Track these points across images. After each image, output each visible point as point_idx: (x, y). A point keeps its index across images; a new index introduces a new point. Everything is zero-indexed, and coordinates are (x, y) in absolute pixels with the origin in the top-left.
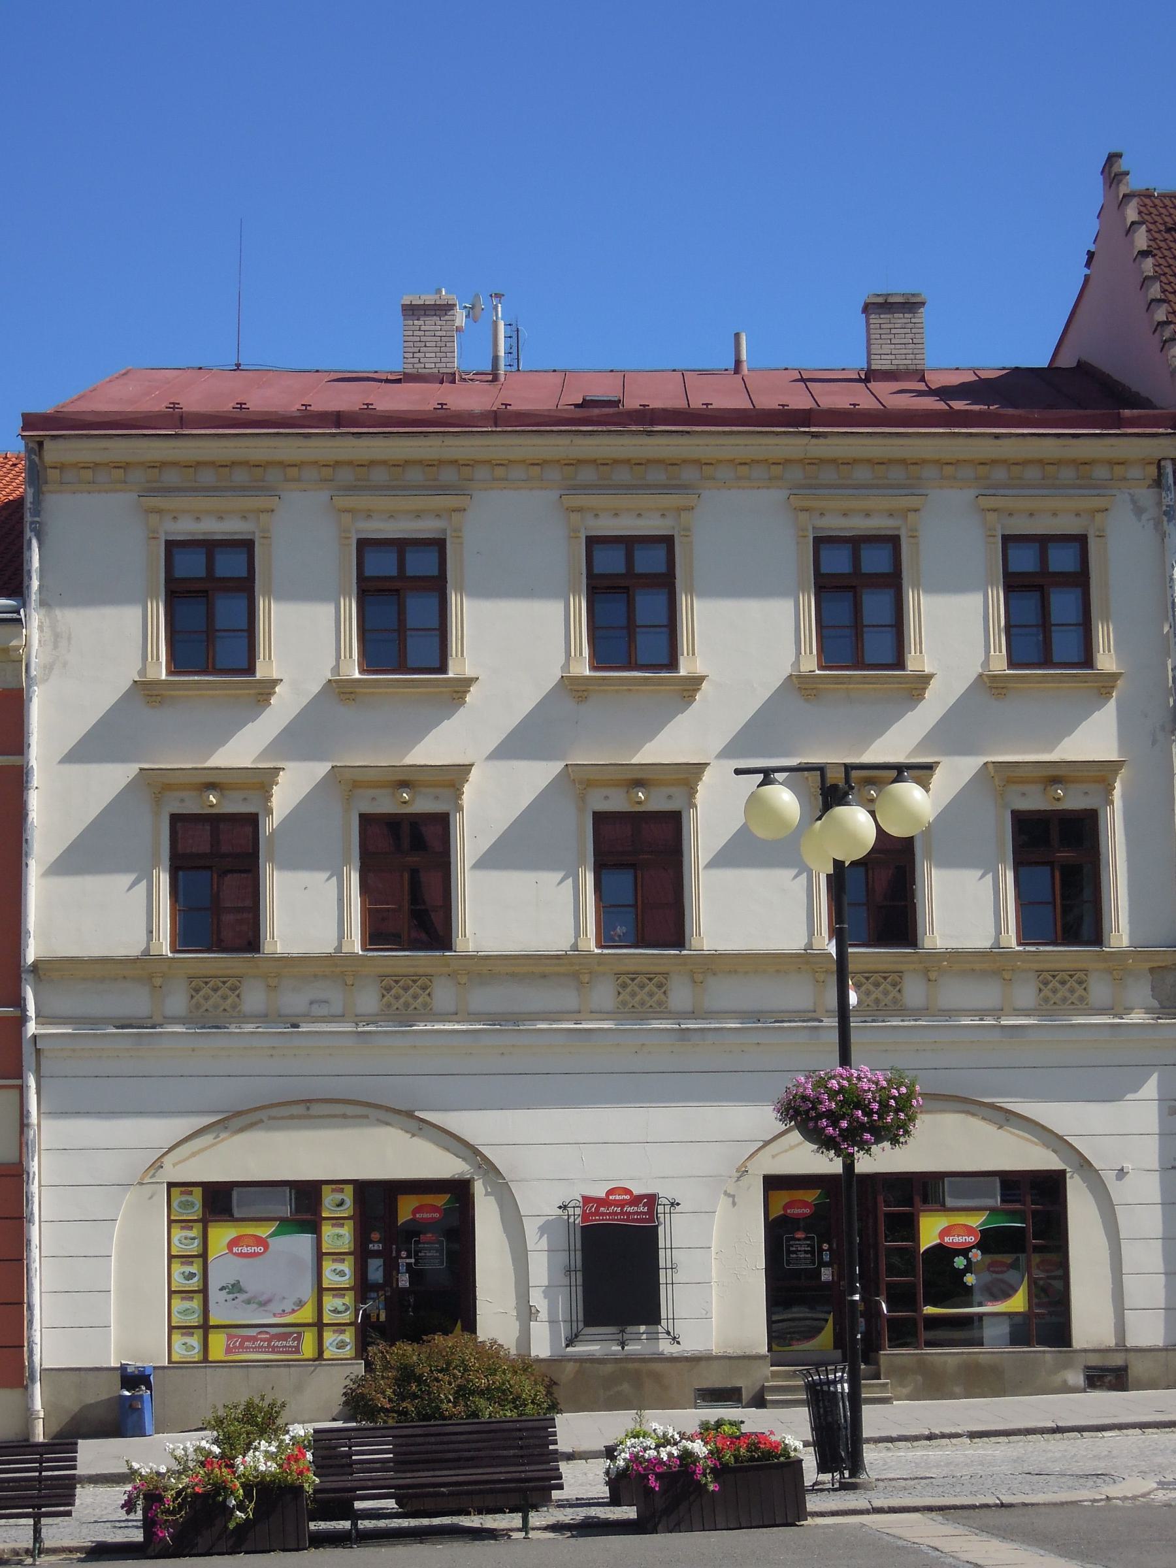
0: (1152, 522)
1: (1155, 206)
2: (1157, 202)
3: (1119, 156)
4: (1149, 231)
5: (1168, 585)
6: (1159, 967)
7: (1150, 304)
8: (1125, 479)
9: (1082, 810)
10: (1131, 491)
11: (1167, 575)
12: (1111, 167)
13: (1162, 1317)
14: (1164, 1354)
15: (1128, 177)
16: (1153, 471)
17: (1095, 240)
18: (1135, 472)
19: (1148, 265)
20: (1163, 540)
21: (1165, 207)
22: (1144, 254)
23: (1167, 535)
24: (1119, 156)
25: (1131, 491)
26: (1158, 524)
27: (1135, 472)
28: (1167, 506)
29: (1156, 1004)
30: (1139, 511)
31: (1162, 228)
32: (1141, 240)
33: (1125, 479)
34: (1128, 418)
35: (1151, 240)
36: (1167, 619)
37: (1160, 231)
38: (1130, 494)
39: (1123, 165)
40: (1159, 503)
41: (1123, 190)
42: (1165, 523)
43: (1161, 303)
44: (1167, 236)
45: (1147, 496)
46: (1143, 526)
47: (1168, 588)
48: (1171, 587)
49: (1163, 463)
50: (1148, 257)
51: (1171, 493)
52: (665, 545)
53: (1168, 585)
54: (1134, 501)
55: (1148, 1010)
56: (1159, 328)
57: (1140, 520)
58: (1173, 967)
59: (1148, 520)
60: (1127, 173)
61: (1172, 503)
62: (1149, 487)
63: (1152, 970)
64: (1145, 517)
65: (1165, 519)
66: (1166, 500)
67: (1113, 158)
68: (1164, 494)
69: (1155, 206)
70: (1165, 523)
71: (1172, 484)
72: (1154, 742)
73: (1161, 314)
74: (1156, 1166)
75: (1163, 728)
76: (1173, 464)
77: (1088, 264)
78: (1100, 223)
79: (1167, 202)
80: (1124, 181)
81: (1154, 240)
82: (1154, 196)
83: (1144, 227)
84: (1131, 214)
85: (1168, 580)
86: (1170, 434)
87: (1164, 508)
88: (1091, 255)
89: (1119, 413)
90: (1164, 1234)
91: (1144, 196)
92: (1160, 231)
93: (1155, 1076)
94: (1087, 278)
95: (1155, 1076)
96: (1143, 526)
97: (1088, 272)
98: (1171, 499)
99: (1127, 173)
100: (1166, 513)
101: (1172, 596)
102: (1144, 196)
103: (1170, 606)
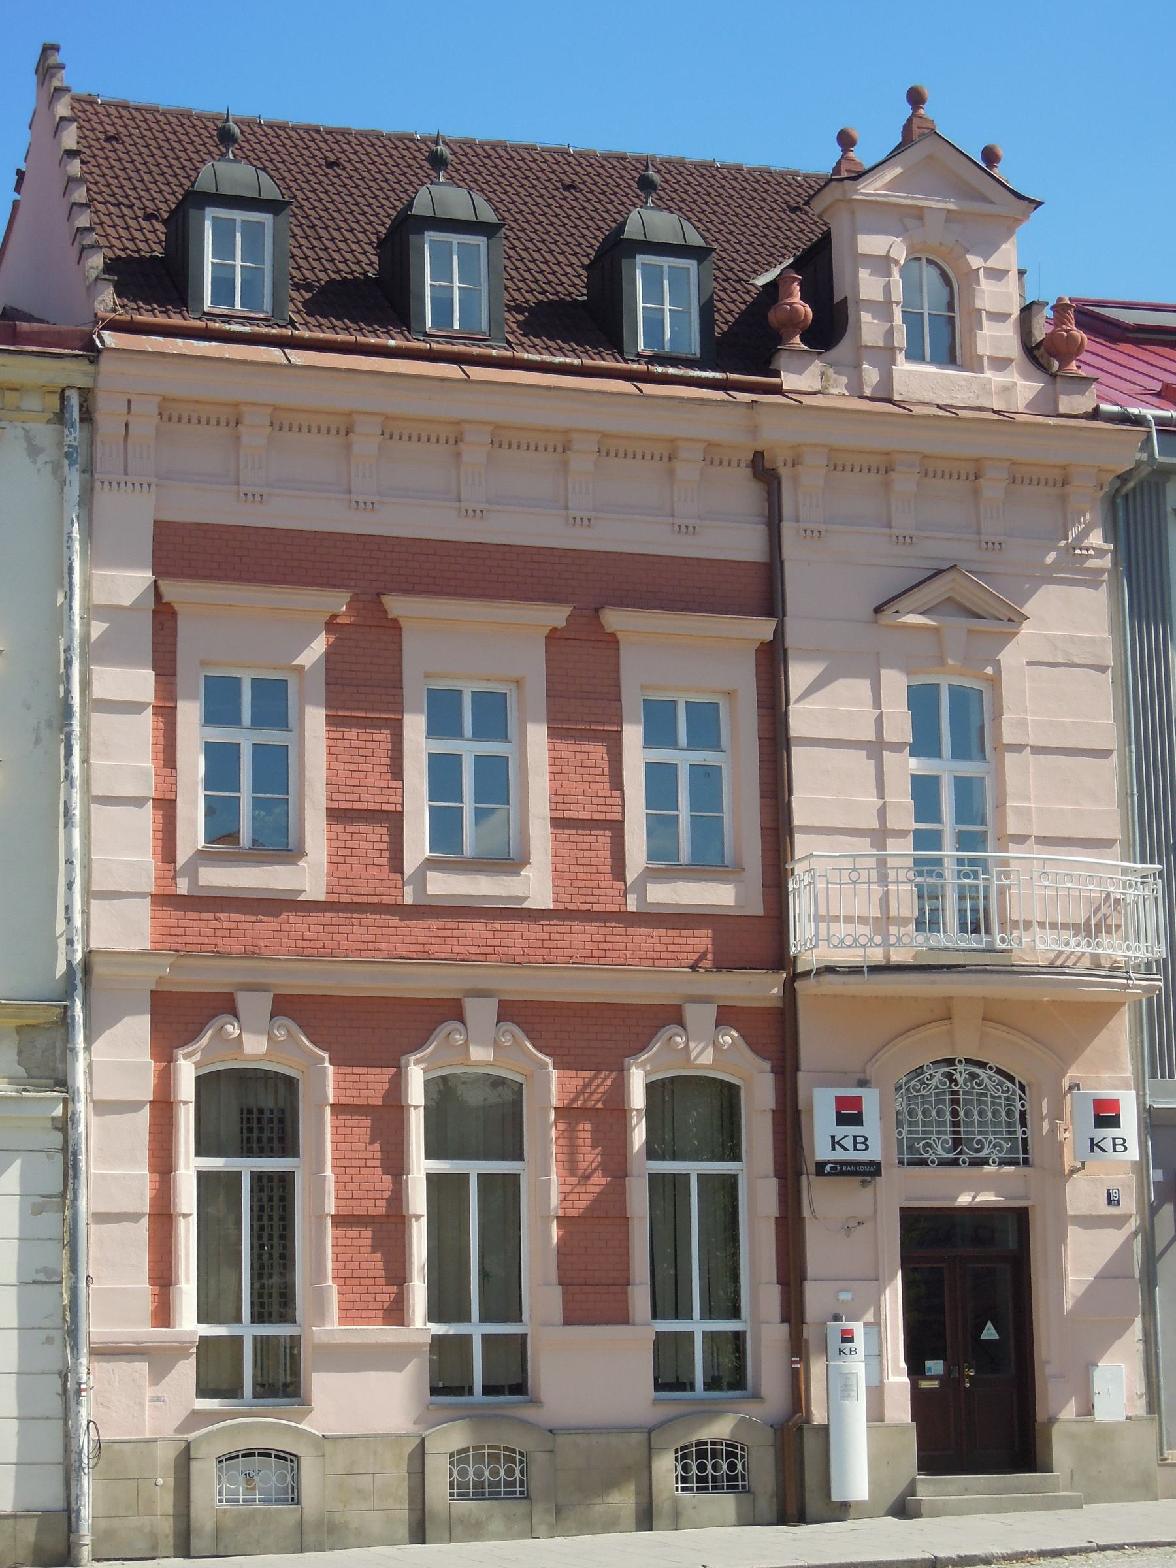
0: (49, 466)
1: (96, 114)
2: (99, 109)
3: (56, 48)
4: (80, 128)
5: (65, 544)
6: (28, 1026)
7: (71, 208)
8: (18, 409)
9: (778, 1268)
10: (27, 426)
11: (66, 532)
12: (44, 63)
13: (13, 1474)
14: (11, 1522)
15: (63, 71)
16: (55, 401)
17: (26, 158)
18: (32, 403)
19: (75, 167)
20: (63, 489)
21: (109, 115)
22: (71, 154)
23: (67, 482)
24: (56, 48)
25: (27, 426)
26: (57, 469)
27: (32, 403)
28: (70, 446)
29: (22, 1071)
30: (34, 451)
31: (102, 136)
32: (70, 138)
33: (18, 409)
34: (25, 332)
35: (80, 137)
36: (62, 586)
37: (98, 140)
38: (23, 428)
39: (58, 58)
40: (60, 444)
41: (56, 83)
42: (66, 468)
43: (84, 209)
44: (144, 224)
45: (44, 433)
46: (39, 470)
47: (65, 548)
48: (68, 547)
49: (67, 393)
50: (75, 158)
51: (75, 431)
52: (942, 1373)
53: (65, 544)
54: (29, 439)
55: (13, 1080)
56: (78, 235)
57: (34, 462)
58: (47, 1026)
59: (46, 463)
60: (62, 67)
61: (75, 443)
62: (49, 422)
63: (19, 1029)
64: (42, 458)
65: (66, 462)
66: (68, 439)
67: (49, 49)
68: (66, 432)
69: (96, 114)
70: (66, 468)
71: (78, 421)
72: (37, 741)
73: (83, 220)
74: (13, 1280)
75: (49, 724)
76: (80, 395)
77: (18, 189)
78: (32, 135)
79: (112, 111)
80: (59, 76)
81: (85, 137)
82: (97, 103)
83: (76, 124)
84: (62, 109)
85: (66, 538)
86: (77, 356)
87: (66, 449)
88: (21, 174)
89: (15, 325)
90: (19, 1366)
91: (84, 101)
92: (98, 140)
93: (17, 1164)
94: (16, 204)
95: (17, 1164)
96: (39, 470)
97: (17, 197)
98: (75, 439)
99: (62, 67)
100: (67, 455)
101: (70, 559)
102: (84, 101)
103: (66, 570)
